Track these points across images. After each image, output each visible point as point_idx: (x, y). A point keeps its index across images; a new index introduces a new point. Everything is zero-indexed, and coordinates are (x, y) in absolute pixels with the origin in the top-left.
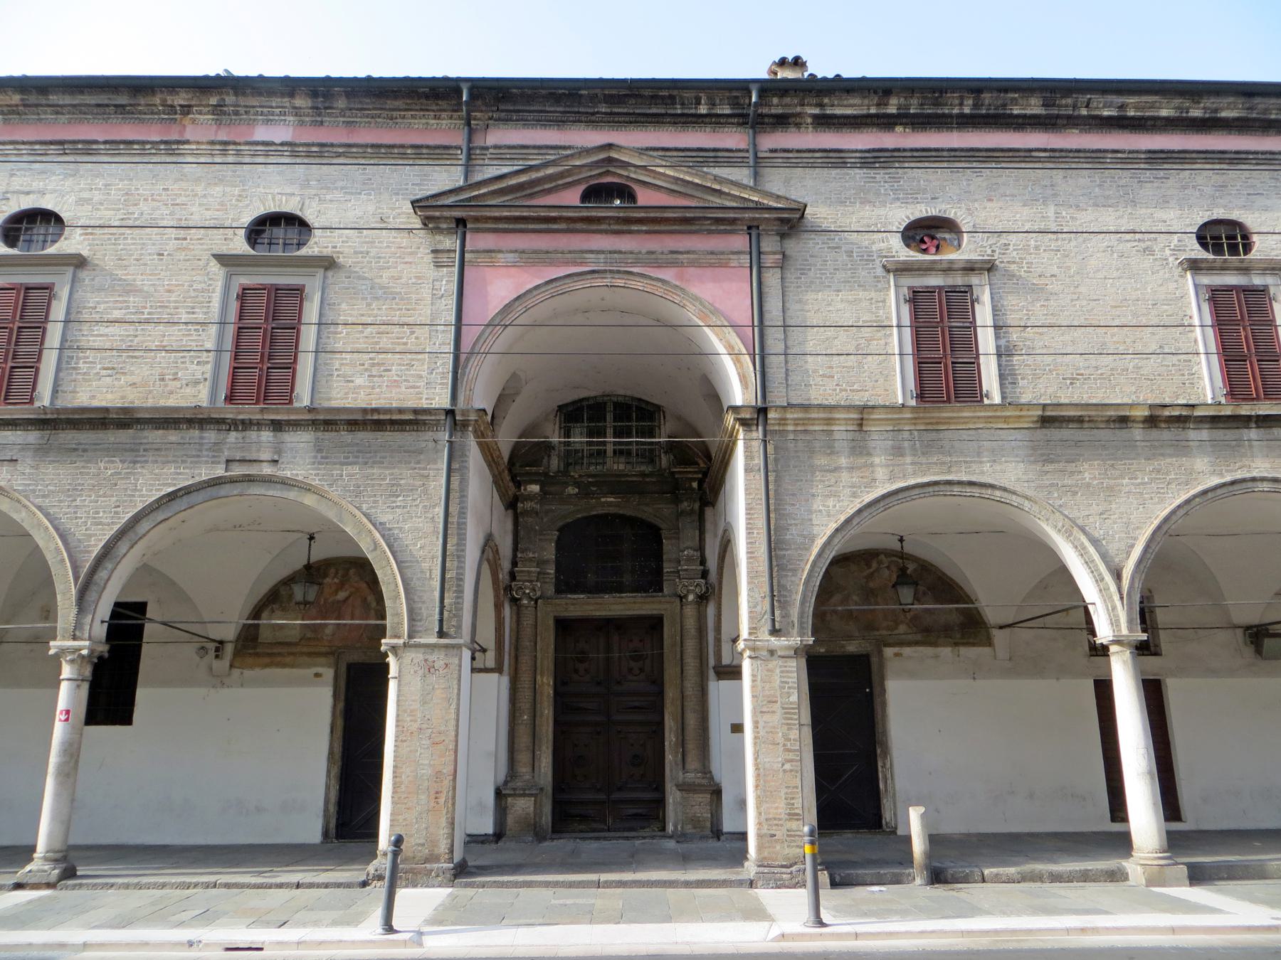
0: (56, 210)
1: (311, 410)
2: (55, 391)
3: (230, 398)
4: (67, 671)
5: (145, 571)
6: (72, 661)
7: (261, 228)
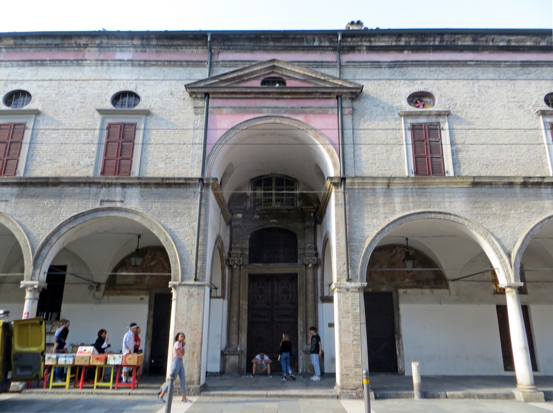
0: (28, 90)
1: (139, 178)
2: (26, 170)
3: (103, 173)
4: (28, 295)
5: (64, 251)
6: (30, 291)
7: (118, 98)
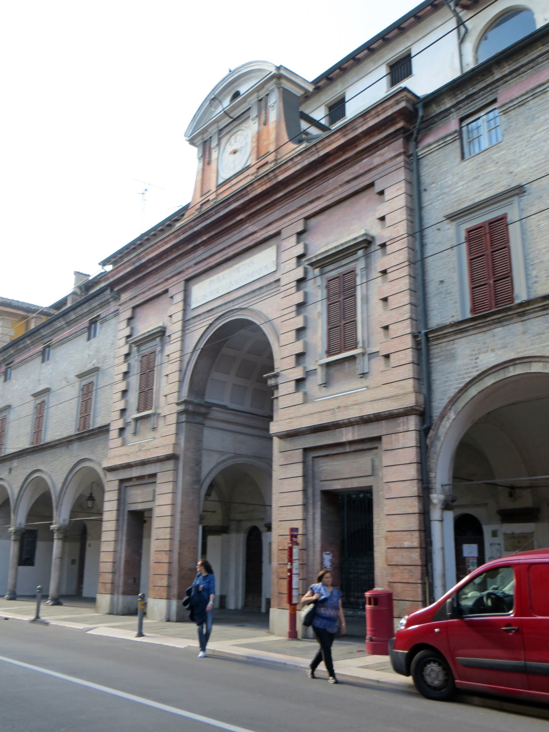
2: (528, 288)
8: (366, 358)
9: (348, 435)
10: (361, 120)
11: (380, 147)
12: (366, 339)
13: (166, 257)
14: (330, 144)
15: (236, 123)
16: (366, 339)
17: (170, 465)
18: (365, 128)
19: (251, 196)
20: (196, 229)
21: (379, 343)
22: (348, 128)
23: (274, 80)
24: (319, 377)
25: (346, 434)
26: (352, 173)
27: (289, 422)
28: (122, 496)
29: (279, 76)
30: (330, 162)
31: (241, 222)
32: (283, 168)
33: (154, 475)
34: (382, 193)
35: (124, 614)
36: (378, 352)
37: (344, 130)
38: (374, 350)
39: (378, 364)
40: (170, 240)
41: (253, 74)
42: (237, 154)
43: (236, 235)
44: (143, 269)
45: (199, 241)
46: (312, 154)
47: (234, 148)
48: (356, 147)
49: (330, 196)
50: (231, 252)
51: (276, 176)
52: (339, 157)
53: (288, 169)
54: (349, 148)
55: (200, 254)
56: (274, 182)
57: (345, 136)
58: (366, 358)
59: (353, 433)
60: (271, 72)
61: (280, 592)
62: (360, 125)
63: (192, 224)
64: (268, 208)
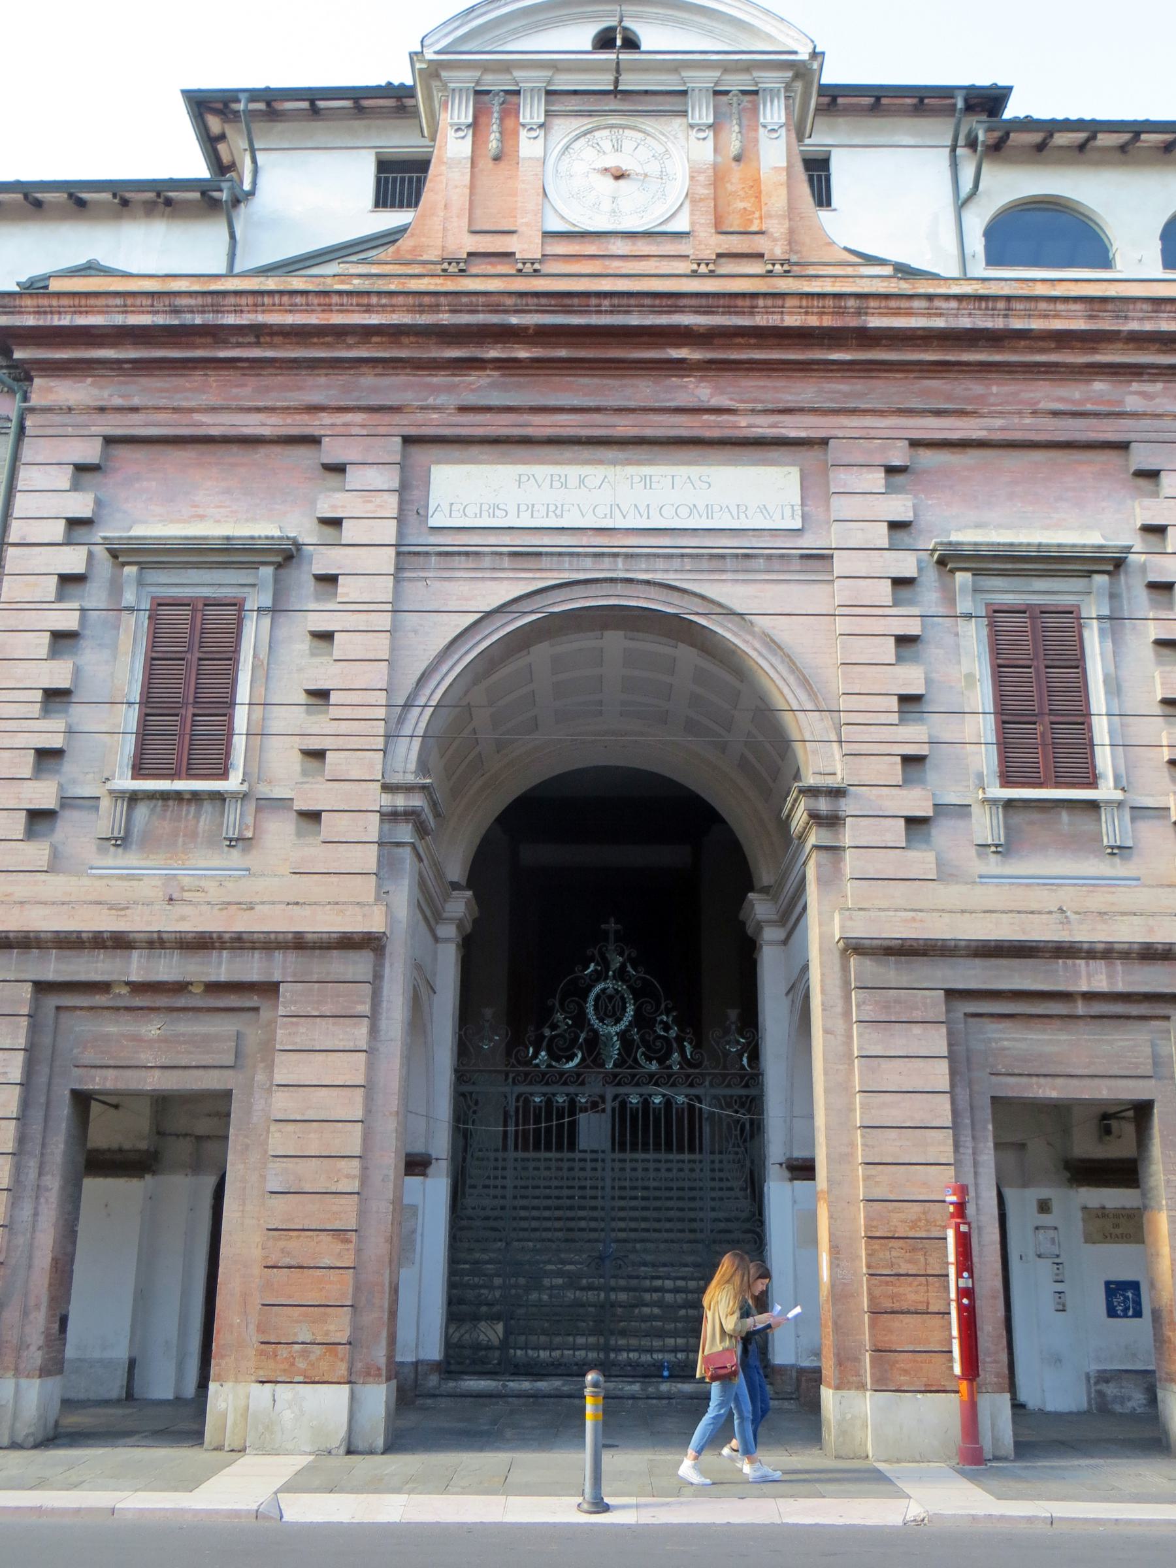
8: (251, 806)
9: (1096, 978)
10: (1147, 307)
11: (1146, 377)
12: (1122, 771)
13: (328, 345)
14: (1046, 316)
15: (612, 104)
16: (1122, 771)
17: (358, 965)
18: (1148, 326)
19: (760, 320)
20: (514, 320)
21: (284, 774)
22: (1110, 307)
23: (790, 74)
24: (107, 819)
25: (1089, 976)
26: (1060, 399)
27: (914, 919)
28: (46, 1040)
29: (801, 71)
30: (1014, 350)
31: (680, 367)
32: (893, 304)
33: (270, 989)
34: (1152, 475)
35: (36, 1446)
36: (292, 799)
37: (1096, 306)
38: (278, 792)
39: (279, 832)
40: (394, 309)
41: (703, 20)
42: (622, 182)
43: (643, 391)
44: (209, 340)
45: (493, 353)
46: (993, 313)
47: (625, 165)
48: (1094, 350)
49: (998, 422)
50: (624, 427)
51: (859, 313)
52: (1042, 351)
53: (909, 313)
54: (1079, 345)
55: (479, 387)
56: (853, 322)
57: (1091, 317)
58: (251, 806)
59: (1110, 977)
60: (795, 53)
61: (881, 1346)
62: (1141, 315)
63: (509, 301)
64: (782, 370)
